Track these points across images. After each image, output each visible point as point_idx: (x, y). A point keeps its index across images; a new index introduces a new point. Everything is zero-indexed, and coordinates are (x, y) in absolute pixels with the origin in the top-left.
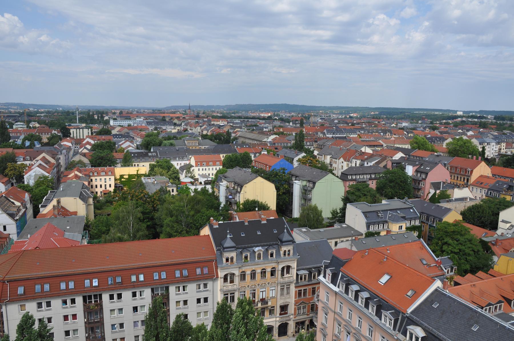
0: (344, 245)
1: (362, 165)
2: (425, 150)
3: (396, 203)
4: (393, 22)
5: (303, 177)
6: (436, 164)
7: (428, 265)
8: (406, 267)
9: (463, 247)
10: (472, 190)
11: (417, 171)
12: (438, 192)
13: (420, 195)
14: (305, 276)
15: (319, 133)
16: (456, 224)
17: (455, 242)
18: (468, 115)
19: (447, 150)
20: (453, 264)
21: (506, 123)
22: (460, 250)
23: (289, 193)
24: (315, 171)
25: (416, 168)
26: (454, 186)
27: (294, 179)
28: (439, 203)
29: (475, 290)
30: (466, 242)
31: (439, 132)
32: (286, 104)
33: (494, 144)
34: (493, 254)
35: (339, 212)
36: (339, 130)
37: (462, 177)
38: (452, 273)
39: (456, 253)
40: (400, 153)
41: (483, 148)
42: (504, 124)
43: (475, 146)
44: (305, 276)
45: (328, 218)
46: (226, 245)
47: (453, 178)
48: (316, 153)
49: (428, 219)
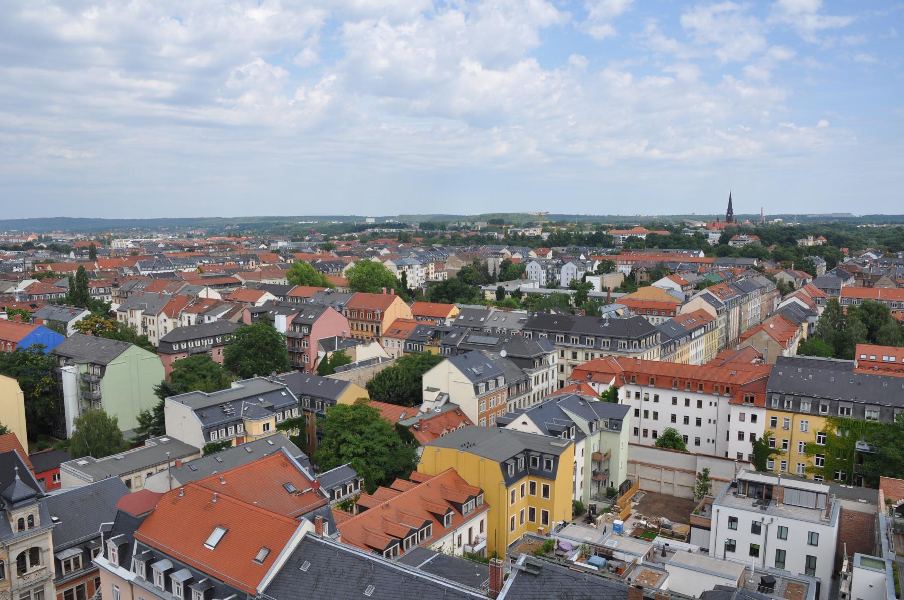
0: (157, 482)
1: (200, 322)
2: (311, 285)
3: (258, 384)
4: (279, 72)
5: (81, 358)
6: (324, 307)
7: (299, 493)
8: (252, 507)
9: (371, 443)
10: (387, 344)
11: (294, 323)
12: (330, 354)
13: (304, 364)
14: (76, 560)
15: (126, 270)
16: (359, 405)
17: (358, 436)
18: (381, 224)
19: (346, 282)
20: (357, 476)
21: (437, 234)
22: (366, 448)
23: (57, 392)
24: (105, 344)
25: (292, 317)
26: (355, 341)
27: (62, 362)
28: (334, 372)
29: (389, 513)
30: (373, 434)
31: (337, 253)
32: (64, 218)
33: (418, 266)
34: (417, 444)
35: (153, 416)
36: (163, 261)
37: (368, 325)
38: (358, 491)
39: (359, 455)
40: (268, 293)
41: (404, 274)
42: (434, 235)
43: (390, 272)
44: (76, 560)
45: (134, 430)
46: (15, 497)
47: (355, 328)
48: (115, 307)
49: (313, 405)
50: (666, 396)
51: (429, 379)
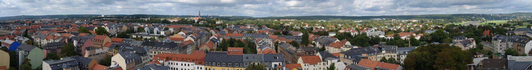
3: (68, 59)
11: (79, 43)
18: (106, 17)
24: (30, 46)
50: (180, 63)
51: (113, 59)
